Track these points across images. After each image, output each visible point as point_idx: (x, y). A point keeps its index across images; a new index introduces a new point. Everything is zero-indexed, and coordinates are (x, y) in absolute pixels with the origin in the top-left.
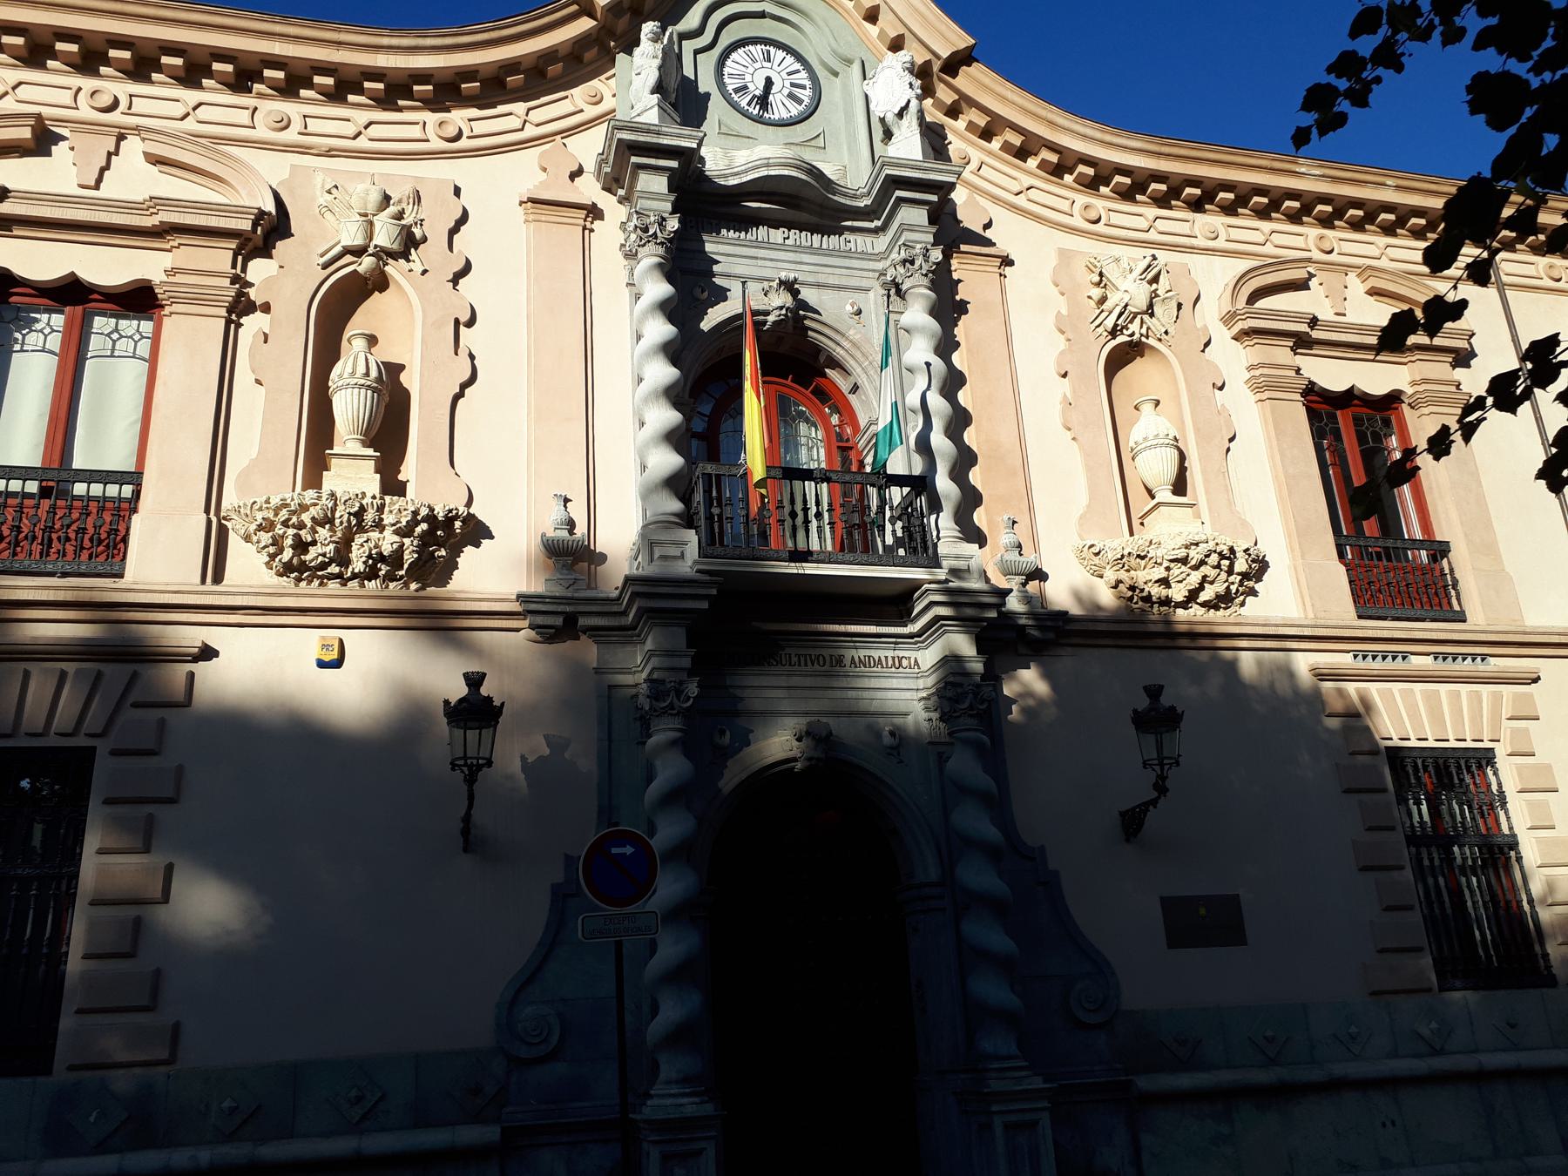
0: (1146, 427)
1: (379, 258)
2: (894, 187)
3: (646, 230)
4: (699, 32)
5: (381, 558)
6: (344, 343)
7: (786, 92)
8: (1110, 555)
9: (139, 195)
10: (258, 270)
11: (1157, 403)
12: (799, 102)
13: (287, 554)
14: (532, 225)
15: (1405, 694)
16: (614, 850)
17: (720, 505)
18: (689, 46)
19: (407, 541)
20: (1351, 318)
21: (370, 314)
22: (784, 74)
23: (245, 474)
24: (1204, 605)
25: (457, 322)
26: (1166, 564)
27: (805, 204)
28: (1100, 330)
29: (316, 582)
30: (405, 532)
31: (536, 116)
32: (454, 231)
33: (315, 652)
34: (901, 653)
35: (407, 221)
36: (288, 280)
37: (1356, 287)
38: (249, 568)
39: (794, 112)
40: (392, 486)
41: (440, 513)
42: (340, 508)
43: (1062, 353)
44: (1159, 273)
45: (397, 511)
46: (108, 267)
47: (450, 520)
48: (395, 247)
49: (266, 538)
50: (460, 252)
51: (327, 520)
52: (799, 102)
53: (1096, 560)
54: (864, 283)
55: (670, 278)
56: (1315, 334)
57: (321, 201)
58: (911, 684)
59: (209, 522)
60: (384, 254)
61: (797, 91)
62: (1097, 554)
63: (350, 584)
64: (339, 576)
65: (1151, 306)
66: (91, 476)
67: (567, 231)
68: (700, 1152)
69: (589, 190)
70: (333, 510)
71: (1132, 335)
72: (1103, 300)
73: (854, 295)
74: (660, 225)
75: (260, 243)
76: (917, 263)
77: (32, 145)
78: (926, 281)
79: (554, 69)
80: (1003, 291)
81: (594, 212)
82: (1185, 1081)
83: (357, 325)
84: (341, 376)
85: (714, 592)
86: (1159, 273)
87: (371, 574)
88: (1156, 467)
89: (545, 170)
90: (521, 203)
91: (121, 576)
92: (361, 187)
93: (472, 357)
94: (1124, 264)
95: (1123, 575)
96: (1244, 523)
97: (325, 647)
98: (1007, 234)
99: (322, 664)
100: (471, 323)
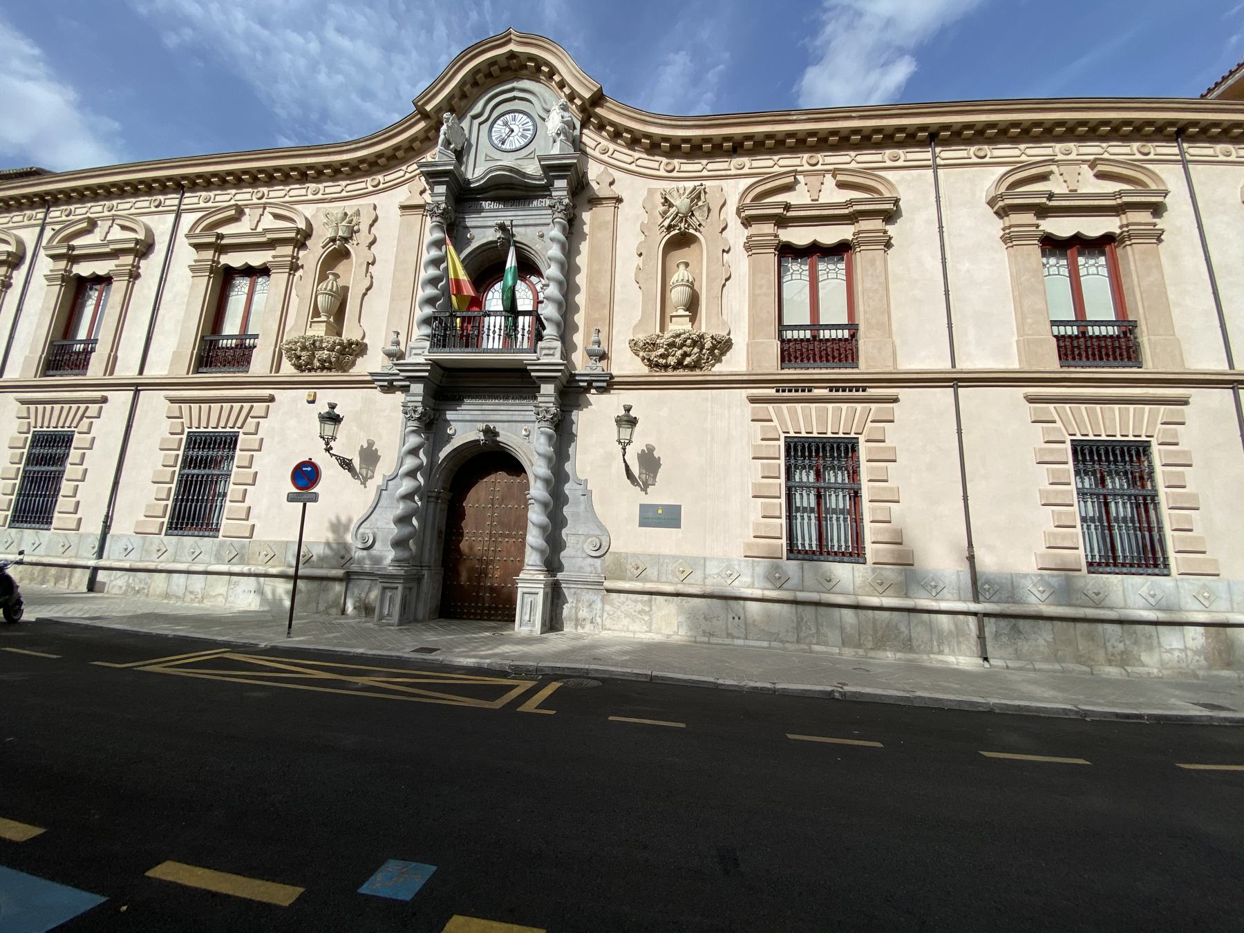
0: (680, 275)
2: (553, 170)
12: (525, 137)
15: (793, 414)
18: (476, 122)
20: (1082, 190)
21: (340, 268)
24: (687, 367)
27: (511, 190)
31: (859, 158)
32: (371, 226)
33: (306, 398)
37: (829, 181)
38: (287, 368)
47: (350, 343)
52: (525, 137)
56: (224, 242)
60: (346, 240)
80: (615, 216)
87: (323, 368)
94: (681, 191)
96: (724, 323)
98: (626, 186)
99: (309, 402)
100: (373, 263)
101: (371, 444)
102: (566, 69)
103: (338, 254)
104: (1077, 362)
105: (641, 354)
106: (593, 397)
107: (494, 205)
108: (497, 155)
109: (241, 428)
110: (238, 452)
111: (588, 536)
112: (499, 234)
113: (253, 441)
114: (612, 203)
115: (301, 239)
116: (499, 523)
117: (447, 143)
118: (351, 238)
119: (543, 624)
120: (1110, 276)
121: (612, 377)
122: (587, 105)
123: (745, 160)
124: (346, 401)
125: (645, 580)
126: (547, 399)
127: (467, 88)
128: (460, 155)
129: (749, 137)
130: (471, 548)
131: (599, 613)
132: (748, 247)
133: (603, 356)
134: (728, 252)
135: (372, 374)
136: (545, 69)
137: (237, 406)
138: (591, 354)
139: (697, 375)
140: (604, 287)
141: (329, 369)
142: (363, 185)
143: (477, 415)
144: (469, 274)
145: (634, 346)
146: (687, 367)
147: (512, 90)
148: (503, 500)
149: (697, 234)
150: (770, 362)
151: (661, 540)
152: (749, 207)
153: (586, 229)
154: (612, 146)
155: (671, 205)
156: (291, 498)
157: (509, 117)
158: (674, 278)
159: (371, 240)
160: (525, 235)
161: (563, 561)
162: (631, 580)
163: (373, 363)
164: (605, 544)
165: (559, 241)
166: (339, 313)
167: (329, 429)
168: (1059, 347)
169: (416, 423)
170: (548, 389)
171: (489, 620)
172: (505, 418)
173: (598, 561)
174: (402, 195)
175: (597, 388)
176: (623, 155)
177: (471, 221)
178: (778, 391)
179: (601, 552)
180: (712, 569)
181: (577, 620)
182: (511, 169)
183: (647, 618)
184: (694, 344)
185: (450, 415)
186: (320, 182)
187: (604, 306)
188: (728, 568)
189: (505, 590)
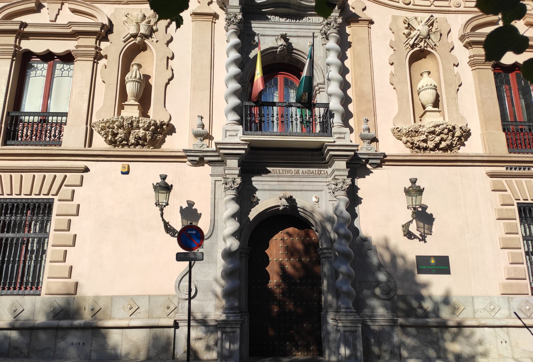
1: (142, 38)
3: (230, 20)
5: (140, 138)
6: (131, 67)
8: (404, 131)
9: (65, 22)
10: (104, 45)
11: (429, 73)
13: (110, 137)
14: (194, 22)
15: (520, 185)
16: (189, 232)
17: (250, 117)
19: (147, 132)
21: (139, 58)
23: (99, 112)
24: (442, 149)
25: (168, 58)
26: (426, 134)
28: (408, 46)
29: (120, 147)
34: (321, 169)
36: (113, 48)
38: (100, 143)
40: (144, 113)
41: (158, 123)
42: (125, 122)
43: (391, 56)
44: (433, 22)
45: (144, 122)
46: (59, 47)
47: (162, 124)
48: (147, 33)
49: (103, 132)
51: (121, 126)
53: (399, 134)
55: (239, 37)
56: (27, 30)
58: (324, 180)
59: (87, 128)
62: (399, 131)
63: (131, 147)
64: (127, 144)
65: (429, 35)
66: (30, 114)
67: (206, 24)
70: (123, 123)
71: (421, 47)
72: (409, 34)
74: (235, 17)
75: (104, 35)
76: (332, 24)
77: (36, 9)
78: (335, 31)
80: (369, 33)
81: (216, 16)
83: (138, 59)
85: (246, 147)
86: (433, 22)
87: (136, 144)
88: (428, 96)
89: (199, 2)
90: (191, 15)
91: (60, 146)
92: (136, 13)
93: (172, 70)
94: (419, 19)
95: (409, 139)
96: (463, 118)
97: (124, 167)
98: (373, 11)
99: (123, 173)
100: (172, 58)
104: (519, 150)
105: (404, 139)
109: (56, 194)
110: (54, 217)
112: (282, 42)
113: (70, 207)
115: (105, 32)
120: (47, 77)
121: (385, 156)
124: (175, 172)
126: (342, 173)
134: (457, 66)
135: (185, 151)
137: (49, 176)
138: (363, 138)
139: (449, 155)
141: (143, 145)
145: (398, 133)
146: (442, 149)
150: (500, 146)
152: (469, 36)
156: (180, 257)
158: (420, 86)
159: (169, 38)
166: (144, 100)
167: (162, 198)
168: (507, 139)
178: (507, 169)
180: (479, 305)
188: (491, 304)
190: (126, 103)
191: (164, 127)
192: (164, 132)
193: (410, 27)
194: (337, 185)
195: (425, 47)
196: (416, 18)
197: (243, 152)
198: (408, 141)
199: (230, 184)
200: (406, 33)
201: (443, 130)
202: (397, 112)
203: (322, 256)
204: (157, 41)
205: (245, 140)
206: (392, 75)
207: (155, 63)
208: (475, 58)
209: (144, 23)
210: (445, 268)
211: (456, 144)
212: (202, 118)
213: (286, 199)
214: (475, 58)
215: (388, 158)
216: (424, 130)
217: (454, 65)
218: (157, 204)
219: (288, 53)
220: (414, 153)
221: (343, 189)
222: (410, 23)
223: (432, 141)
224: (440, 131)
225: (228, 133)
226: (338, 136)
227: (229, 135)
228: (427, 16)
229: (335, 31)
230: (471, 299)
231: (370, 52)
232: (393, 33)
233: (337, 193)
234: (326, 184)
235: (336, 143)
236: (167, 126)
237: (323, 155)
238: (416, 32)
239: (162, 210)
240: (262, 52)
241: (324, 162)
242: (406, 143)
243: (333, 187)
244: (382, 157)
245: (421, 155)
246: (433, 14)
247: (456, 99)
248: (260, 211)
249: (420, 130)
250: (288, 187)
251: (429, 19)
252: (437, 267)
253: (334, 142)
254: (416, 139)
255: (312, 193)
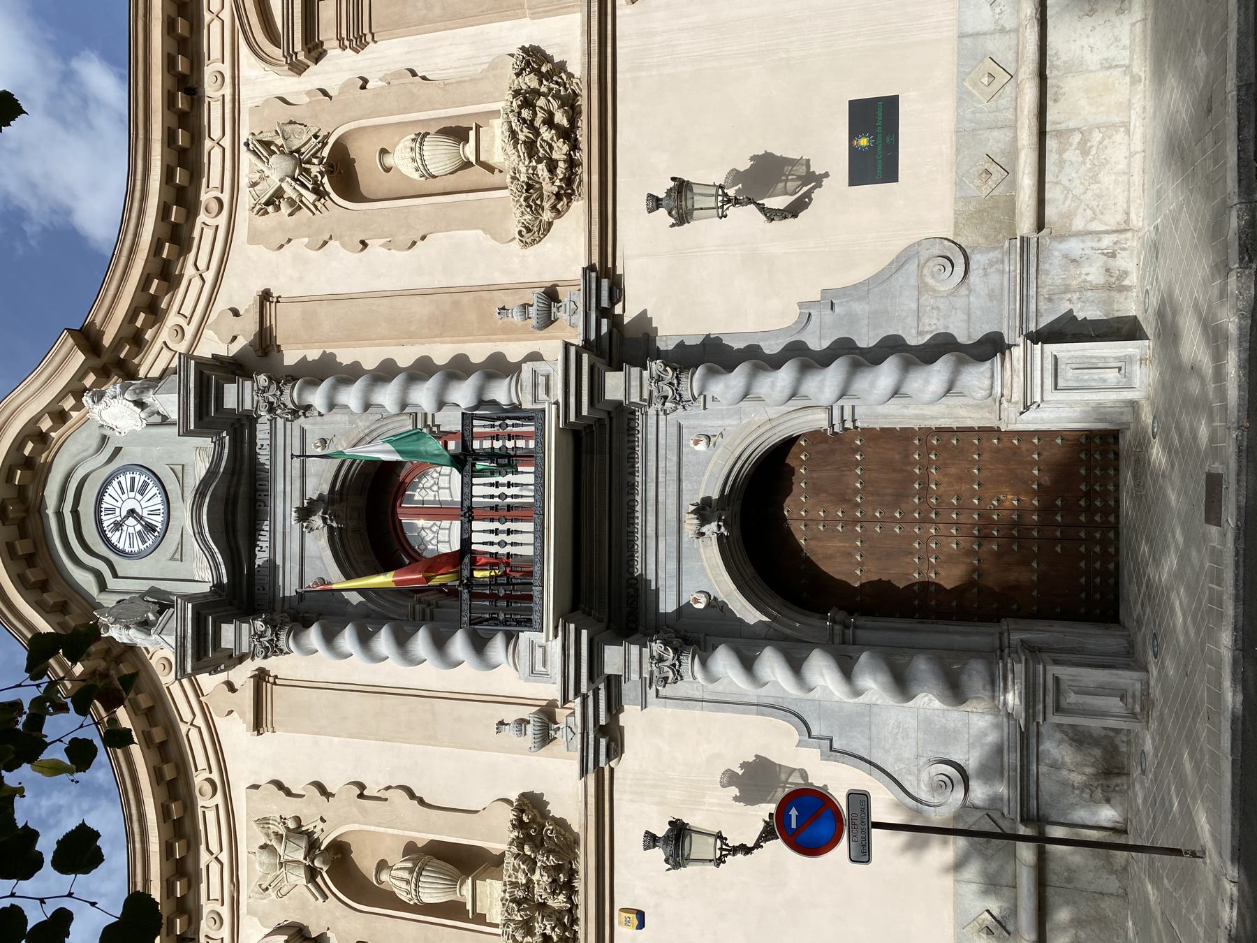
2: (207, 414)
4: (98, 575)
7: (139, 497)
8: (528, 217)
12: (145, 485)
16: (794, 825)
21: (365, 862)
22: (124, 497)
25: (361, 796)
27: (236, 503)
30: (531, 863)
31: (187, 716)
32: (288, 793)
35: (282, 831)
39: (155, 490)
43: (344, 245)
44: (260, 141)
47: (519, 824)
48: (303, 844)
50: (304, 789)
52: (145, 485)
54: (297, 433)
55: (307, 625)
57: (274, 895)
60: (313, 845)
61: (138, 485)
62: (529, 230)
67: (279, 699)
68: (1057, 680)
69: (242, 675)
72: (291, 202)
73: (311, 448)
74: (261, 636)
76: (271, 399)
79: (169, 772)
80: (292, 300)
81: (261, 677)
82: (1027, 182)
84: (409, 892)
85: (572, 626)
86: (260, 141)
88: (439, 155)
93: (389, 788)
94: (256, 177)
95: (547, 205)
96: (493, 66)
97: (627, 923)
98: (240, 290)
99: (641, 925)
100: (362, 786)
101: (730, 778)
102: (31, 401)
103: (336, 866)
105: (547, 216)
106: (629, 310)
107: (264, 542)
108: (173, 537)
111: (922, 288)
112: (317, 521)
114: (271, 309)
116: (895, 505)
117: (145, 626)
118: (309, 834)
119: (1127, 667)
121: (590, 268)
122: (97, 362)
123: (209, 72)
124: (637, 815)
125: (1013, 153)
126: (635, 383)
127: (49, 598)
128: (163, 603)
129: (170, 63)
130: (951, 559)
131: (1090, 242)
132: (358, 40)
133: (551, 295)
135: (584, 772)
136: (28, 449)
138: (547, 321)
139: (589, 104)
140: (420, 308)
141: (572, 874)
142: (211, 815)
143: (667, 544)
144: (385, 569)
145: (534, 233)
146: (573, 121)
147: (59, 515)
148: (844, 499)
149: (331, 141)
151: (922, 138)
153: (313, 355)
154: (172, 320)
155: (279, 193)
157: (107, 521)
160: (320, 476)
161: (977, 336)
162: (1013, 185)
163: (560, 780)
164: (937, 250)
165: (334, 389)
166: (463, 861)
167: (701, 847)
169: (686, 659)
170: (615, 385)
171: (1116, 510)
172: (673, 488)
173: (976, 259)
174: (234, 730)
175: (613, 300)
176: (185, 301)
177: (289, 586)
179: (958, 256)
181: (1109, 287)
182: (197, 506)
183: (1097, 136)
184: (528, 103)
185: (668, 604)
186: (199, 908)
187: (456, 304)
189: (1046, 480)
190: (469, 907)
191: (525, 819)
192: (539, 819)
193: (274, 200)
194: (666, 397)
195: (320, 163)
196: (254, 185)
197: (584, 633)
198: (554, 207)
199: (666, 669)
200: (290, 211)
201: (524, 121)
202: (480, 232)
203: (849, 425)
204: (322, 820)
205: (556, 628)
206: (388, 246)
207: (372, 828)
208: (344, 35)
209: (280, 850)
210: (880, 110)
211: (557, 83)
212: (501, 723)
213: (702, 525)
214: (344, 35)
215: (595, 260)
216: (523, 169)
217: (363, 87)
218: (719, 861)
219: (341, 501)
220: (584, 189)
221: (675, 382)
222: (263, 201)
223: (551, 148)
224: (525, 130)
225: (539, 667)
226: (542, 395)
227: (544, 664)
228: (246, 157)
229: (287, 390)
230: (967, 41)
231: (335, 298)
232: (289, 240)
233: (687, 396)
234: (662, 417)
235: (561, 401)
236: (522, 811)
237: (590, 426)
238: (284, 185)
239: (734, 850)
240: (348, 577)
241: (607, 422)
242: (558, 212)
243: (668, 405)
244: (593, 274)
245: (589, 175)
246: (243, 140)
247: (445, 84)
248: (733, 587)
249: (523, 178)
250: (672, 514)
251: (254, 152)
252: (879, 130)
253: (557, 403)
254: (549, 188)
255: (685, 450)
